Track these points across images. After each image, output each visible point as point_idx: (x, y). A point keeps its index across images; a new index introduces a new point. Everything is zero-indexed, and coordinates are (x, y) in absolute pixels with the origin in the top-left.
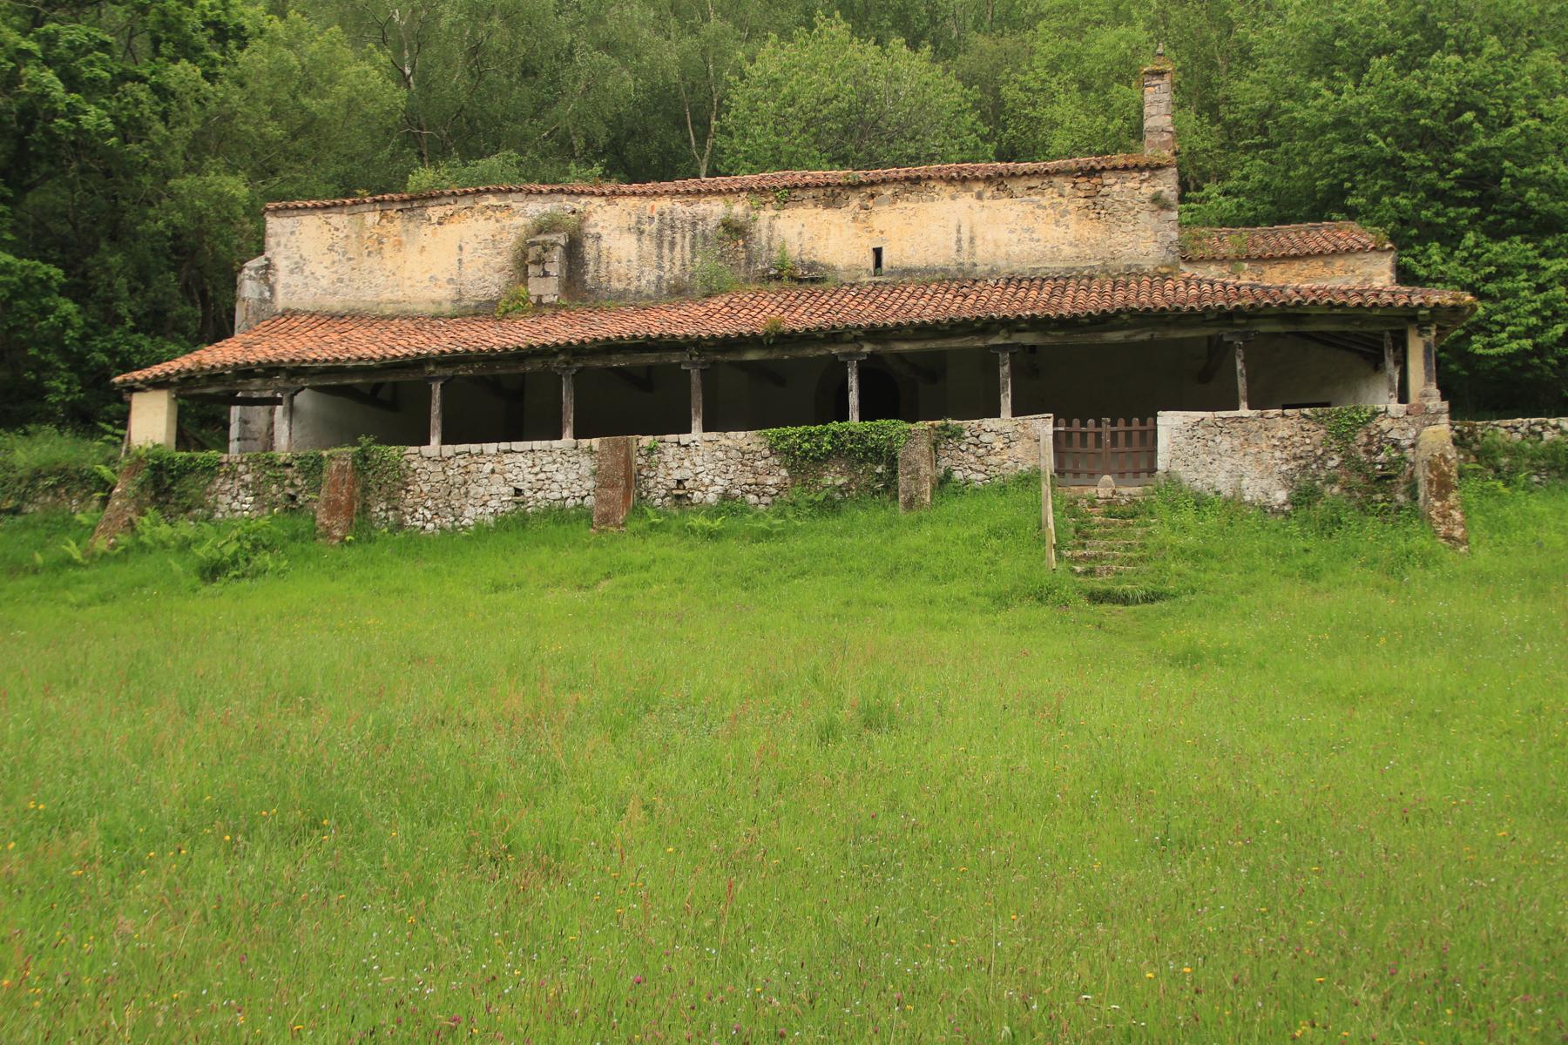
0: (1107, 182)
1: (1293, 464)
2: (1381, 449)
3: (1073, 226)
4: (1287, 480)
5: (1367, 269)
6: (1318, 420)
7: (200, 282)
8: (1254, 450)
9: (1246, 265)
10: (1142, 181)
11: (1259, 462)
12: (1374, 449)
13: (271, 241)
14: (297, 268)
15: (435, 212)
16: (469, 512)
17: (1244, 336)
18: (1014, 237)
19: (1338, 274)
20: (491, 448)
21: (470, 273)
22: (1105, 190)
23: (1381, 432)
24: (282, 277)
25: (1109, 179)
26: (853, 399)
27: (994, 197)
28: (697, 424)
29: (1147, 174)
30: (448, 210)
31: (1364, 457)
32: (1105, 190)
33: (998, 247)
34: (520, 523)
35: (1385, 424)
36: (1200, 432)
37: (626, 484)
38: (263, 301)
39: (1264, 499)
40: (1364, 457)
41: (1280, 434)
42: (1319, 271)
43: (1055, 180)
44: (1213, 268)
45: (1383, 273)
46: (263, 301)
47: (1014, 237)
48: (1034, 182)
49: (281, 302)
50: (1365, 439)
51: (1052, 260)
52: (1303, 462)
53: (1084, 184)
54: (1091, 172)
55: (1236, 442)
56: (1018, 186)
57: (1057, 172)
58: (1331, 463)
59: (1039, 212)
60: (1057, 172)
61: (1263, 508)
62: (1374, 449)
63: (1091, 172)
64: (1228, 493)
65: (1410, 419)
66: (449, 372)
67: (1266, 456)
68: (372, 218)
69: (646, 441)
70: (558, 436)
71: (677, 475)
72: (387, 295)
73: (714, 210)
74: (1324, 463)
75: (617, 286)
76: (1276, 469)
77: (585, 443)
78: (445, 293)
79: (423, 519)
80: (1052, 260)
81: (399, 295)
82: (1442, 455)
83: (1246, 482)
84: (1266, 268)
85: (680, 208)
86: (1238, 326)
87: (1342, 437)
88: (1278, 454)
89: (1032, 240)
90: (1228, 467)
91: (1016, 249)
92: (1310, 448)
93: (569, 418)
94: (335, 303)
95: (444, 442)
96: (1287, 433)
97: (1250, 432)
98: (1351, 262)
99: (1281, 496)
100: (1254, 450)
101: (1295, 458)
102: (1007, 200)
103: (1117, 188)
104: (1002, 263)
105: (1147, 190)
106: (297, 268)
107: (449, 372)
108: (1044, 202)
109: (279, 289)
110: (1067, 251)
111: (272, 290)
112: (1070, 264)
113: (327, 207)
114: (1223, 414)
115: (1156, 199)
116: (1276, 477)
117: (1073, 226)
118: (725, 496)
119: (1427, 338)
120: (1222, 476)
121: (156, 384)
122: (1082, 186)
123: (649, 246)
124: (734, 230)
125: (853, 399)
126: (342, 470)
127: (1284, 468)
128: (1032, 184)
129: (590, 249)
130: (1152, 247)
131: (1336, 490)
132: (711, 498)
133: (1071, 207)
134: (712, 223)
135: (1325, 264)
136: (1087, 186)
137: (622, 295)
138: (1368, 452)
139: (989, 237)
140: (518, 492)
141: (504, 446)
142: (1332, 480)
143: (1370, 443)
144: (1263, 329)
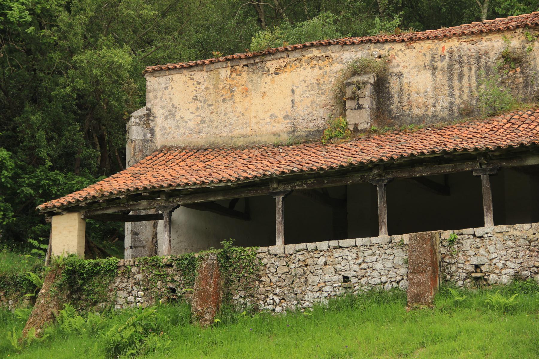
7: (99, 130)
13: (150, 96)
14: (171, 115)
15: (272, 64)
16: (309, 296)
20: (323, 245)
21: (301, 110)
24: (159, 122)
28: (488, 219)
30: (282, 62)
34: (349, 303)
37: (434, 269)
38: (146, 141)
46: (146, 141)
49: (160, 141)
66: (288, 188)
68: (225, 73)
69: (447, 234)
71: (475, 261)
72: (238, 131)
73: (495, 45)
75: (416, 112)
78: (282, 127)
79: (273, 303)
81: (247, 130)
85: (465, 46)
93: (280, 228)
94: (199, 140)
106: (171, 115)
107: (288, 188)
109: (157, 131)
111: (152, 132)
118: (517, 277)
121: (70, 209)
123: (442, 79)
124: (512, 60)
126: (210, 267)
129: (394, 85)
132: (505, 279)
134: (493, 56)
137: (421, 119)
140: (346, 279)
141: (333, 243)
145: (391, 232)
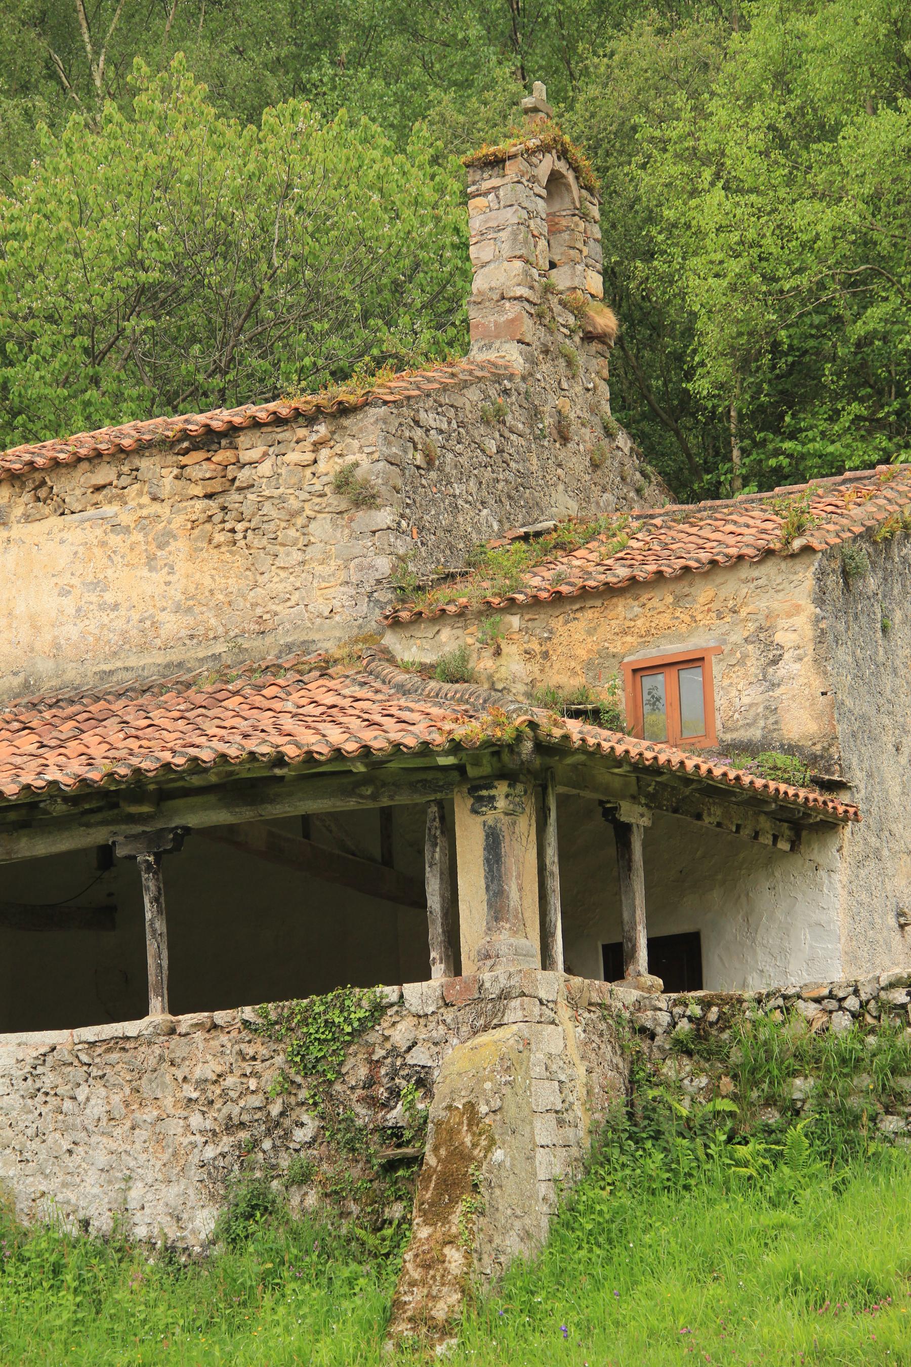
0: (246, 456)
1: (227, 1142)
2: (395, 1093)
3: (182, 567)
4: (215, 1176)
5: (762, 604)
6: (267, 1031)
8: (150, 1114)
9: (515, 621)
10: (317, 446)
11: (160, 1139)
12: (382, 1092)
17: (152, 840)
18: (69, 604)
19: (705, 620)
22: (244, 476)
23: (394, 1052)
25: (251, 448)
26: (156, 957)
27: (28, 518)
29: (322, 429)
31: (363, 1115)
32: (244, 476)
33: (36, 629)
35: (401, 1034)
36: (49, 1080)
39: (173, 1233)
40: (363, 1115)
41: (198, 1073)
42: (666, 619)
43: (144, 464)
44: (446, 634)
45: (798, 609)
47: (69, 604)
48: (105, 474)
50: (363, 1072)
51: (143, 648)
52: (243, 1135)
53: (200, 467)
54: (210, 439)
55: (116, 1099)
56: (72, 487)
57: (143, 448)
58: (300, 1135)
59: (115, 540)
60: (143, 448)
61: (170, 1251)
62: (382, 1092)
63: (210, 439)
64: (102, 1223)
65: (449, 1015)
67: (174, 1127)
70: (141, 1012)
74: (287, 1135)
76: (194, 1159)
77: (187, 1020)
80: (143, 648)
82: (471, 1107)
83: (136, 1193)
84: (557, 624)
86: (132, 819)
87: (314, 1067)
88: (196, 1120)
89: (102, 607)
90: (102, 1159)
91: (72, 631)
92: (256, 1101)
95: (175, 1008)
96: (207, 1069)
97: (141, 1074)
98: (730, 587)
99: (204, 1221)
100: (150, 1114)
101: (231, 1126)
102: (55, 521)
103: (265, 468)
104: (45, 666)
105: (329, 465)
108: (126, 518)
110: (172, 625)
112: (174, 656)
113: (278, 421)
114: (89, 1033)
115: (343, 483)
116: (195, 1174)
117: (182, 567)
119: (490, 817)
120: (92, 1184)
122: (195, 473)
125: (156, 957)
127: (210, 1152)
128: (99, 479)
130: (340, 596)
131: (312, 1200)
133: (179, 521)
135: (678, 600)
136: (207, 470)
138: (372, 1102)
139: (20, 609)
142: (303, 1178)
143: (370, 1082)
144: (193, 820)
145: (175, 1008)
